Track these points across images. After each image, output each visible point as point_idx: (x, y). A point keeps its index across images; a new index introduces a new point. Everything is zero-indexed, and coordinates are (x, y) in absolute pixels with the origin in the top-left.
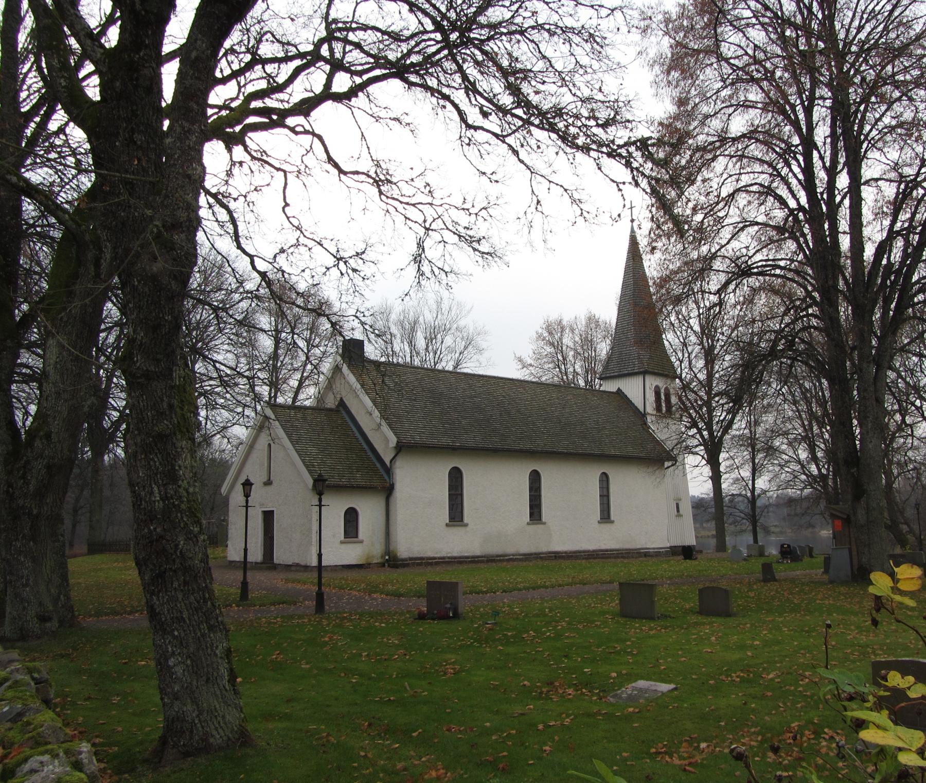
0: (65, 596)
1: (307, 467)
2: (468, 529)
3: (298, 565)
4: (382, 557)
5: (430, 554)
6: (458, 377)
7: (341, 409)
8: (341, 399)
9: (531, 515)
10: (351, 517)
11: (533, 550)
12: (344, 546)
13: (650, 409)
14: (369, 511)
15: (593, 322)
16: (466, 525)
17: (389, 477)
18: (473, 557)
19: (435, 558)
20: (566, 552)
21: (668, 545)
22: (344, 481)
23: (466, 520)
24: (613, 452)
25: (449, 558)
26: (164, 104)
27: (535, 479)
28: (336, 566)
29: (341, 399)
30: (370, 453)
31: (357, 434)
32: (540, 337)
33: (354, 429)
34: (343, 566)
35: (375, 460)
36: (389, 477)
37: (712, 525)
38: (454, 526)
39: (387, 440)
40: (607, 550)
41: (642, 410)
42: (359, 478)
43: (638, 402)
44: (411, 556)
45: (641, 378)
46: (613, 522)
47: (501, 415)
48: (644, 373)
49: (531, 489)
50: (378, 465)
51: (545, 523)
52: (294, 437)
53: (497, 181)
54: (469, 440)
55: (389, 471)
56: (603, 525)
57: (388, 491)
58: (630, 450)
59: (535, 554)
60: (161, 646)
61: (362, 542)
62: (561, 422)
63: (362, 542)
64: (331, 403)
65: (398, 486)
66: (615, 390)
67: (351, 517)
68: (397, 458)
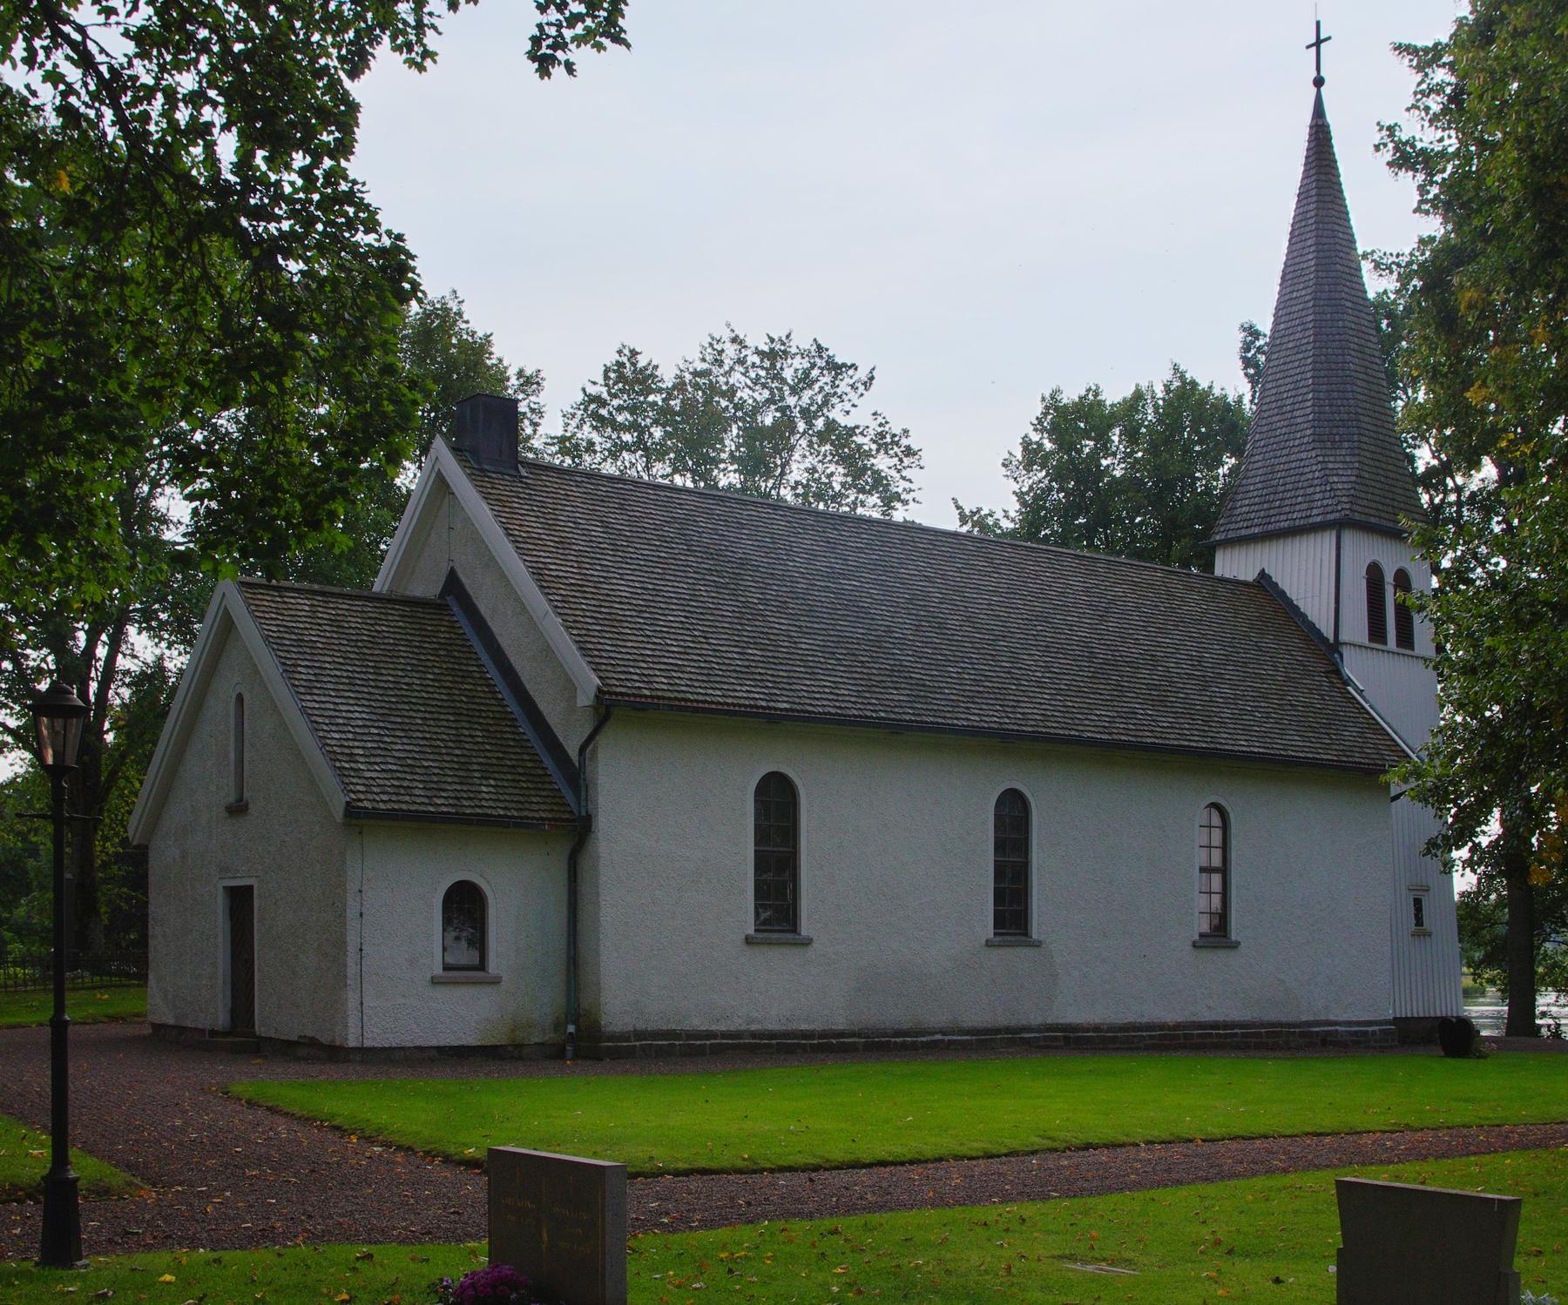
0: (392, 401)
1: (333, 757)
2: (810, 952)
3: (313, 1043)
4: (558, 1026)
5: (698, 1023)
6: (1338, 1290)
7: (450, 600)
8: (452, 572)
9: (999, 921)
10: (465, 907)
11: (1001, 1018)
12: (443, 993)
13: (1355, 626)
14: (515, 887)
15: (1186, 398)
16: (807, 942)
17: (578, 798)
18: (824, 1034)
19: (710, 1035)
20: (1097, 1028)
21: (1390, 1014)
22: (442, 804)
23: (805, 928)
24: (1243, 745)
25: (754, 1035)
26: (1376, 285)
27: (1013, 820)
28: (420, 1049)
29: (452, 572)
30: (525, 729)
31: (493, 673)
32: (1032, 456)
33: (485, 658)
34: (439, 1049)
35: (539, 748)
36: (578, 798)
37: (51, 996)
38: (770, 943)
39: (569, 687)
40: (1215, 1025)
41: (1328, 633)
42: (487, 796)
43: (1318, 612)
44: (641, 1026)
45: (1327, 541)
46: (1235, 946)
47: (918, 628)
48: (1339, 526)
49: (999, 846)
50: (548, 762)
51: (1037, 945)
52: (304, 674)
53: (728, 325)
54: (819, 694)
55: (577, 777)
56: (1207, 955)
57: (577, 831)
58: (1294, 743)
59: (1008, 1030)
60: (108, 312)
61: (496, 981)
62: (1092, 655)
63: (496, 981)
64: (427, 586)
65: (604, 823)
66: (1249, 575)
67: (465, 907)
68: (601, 740)
